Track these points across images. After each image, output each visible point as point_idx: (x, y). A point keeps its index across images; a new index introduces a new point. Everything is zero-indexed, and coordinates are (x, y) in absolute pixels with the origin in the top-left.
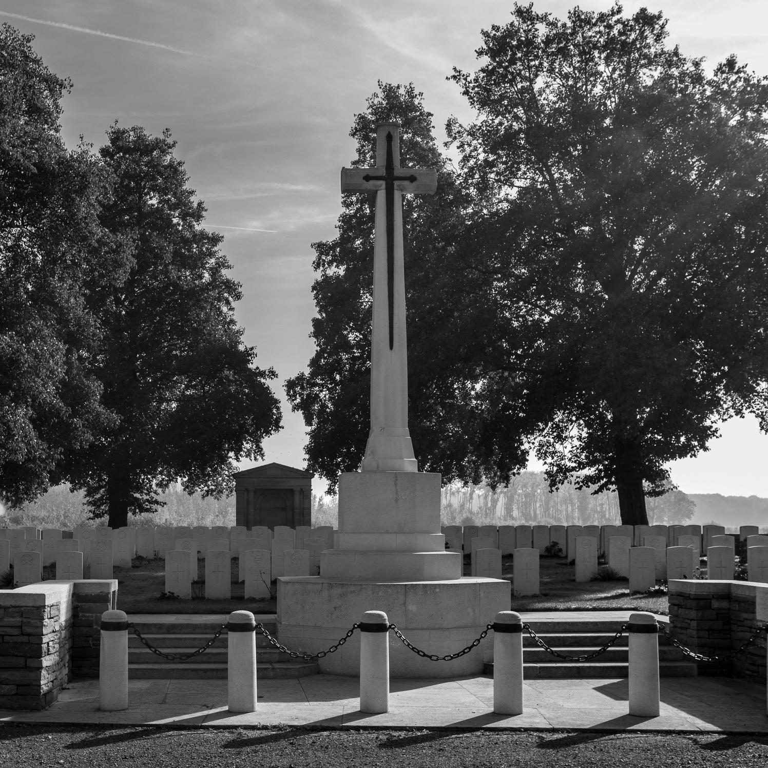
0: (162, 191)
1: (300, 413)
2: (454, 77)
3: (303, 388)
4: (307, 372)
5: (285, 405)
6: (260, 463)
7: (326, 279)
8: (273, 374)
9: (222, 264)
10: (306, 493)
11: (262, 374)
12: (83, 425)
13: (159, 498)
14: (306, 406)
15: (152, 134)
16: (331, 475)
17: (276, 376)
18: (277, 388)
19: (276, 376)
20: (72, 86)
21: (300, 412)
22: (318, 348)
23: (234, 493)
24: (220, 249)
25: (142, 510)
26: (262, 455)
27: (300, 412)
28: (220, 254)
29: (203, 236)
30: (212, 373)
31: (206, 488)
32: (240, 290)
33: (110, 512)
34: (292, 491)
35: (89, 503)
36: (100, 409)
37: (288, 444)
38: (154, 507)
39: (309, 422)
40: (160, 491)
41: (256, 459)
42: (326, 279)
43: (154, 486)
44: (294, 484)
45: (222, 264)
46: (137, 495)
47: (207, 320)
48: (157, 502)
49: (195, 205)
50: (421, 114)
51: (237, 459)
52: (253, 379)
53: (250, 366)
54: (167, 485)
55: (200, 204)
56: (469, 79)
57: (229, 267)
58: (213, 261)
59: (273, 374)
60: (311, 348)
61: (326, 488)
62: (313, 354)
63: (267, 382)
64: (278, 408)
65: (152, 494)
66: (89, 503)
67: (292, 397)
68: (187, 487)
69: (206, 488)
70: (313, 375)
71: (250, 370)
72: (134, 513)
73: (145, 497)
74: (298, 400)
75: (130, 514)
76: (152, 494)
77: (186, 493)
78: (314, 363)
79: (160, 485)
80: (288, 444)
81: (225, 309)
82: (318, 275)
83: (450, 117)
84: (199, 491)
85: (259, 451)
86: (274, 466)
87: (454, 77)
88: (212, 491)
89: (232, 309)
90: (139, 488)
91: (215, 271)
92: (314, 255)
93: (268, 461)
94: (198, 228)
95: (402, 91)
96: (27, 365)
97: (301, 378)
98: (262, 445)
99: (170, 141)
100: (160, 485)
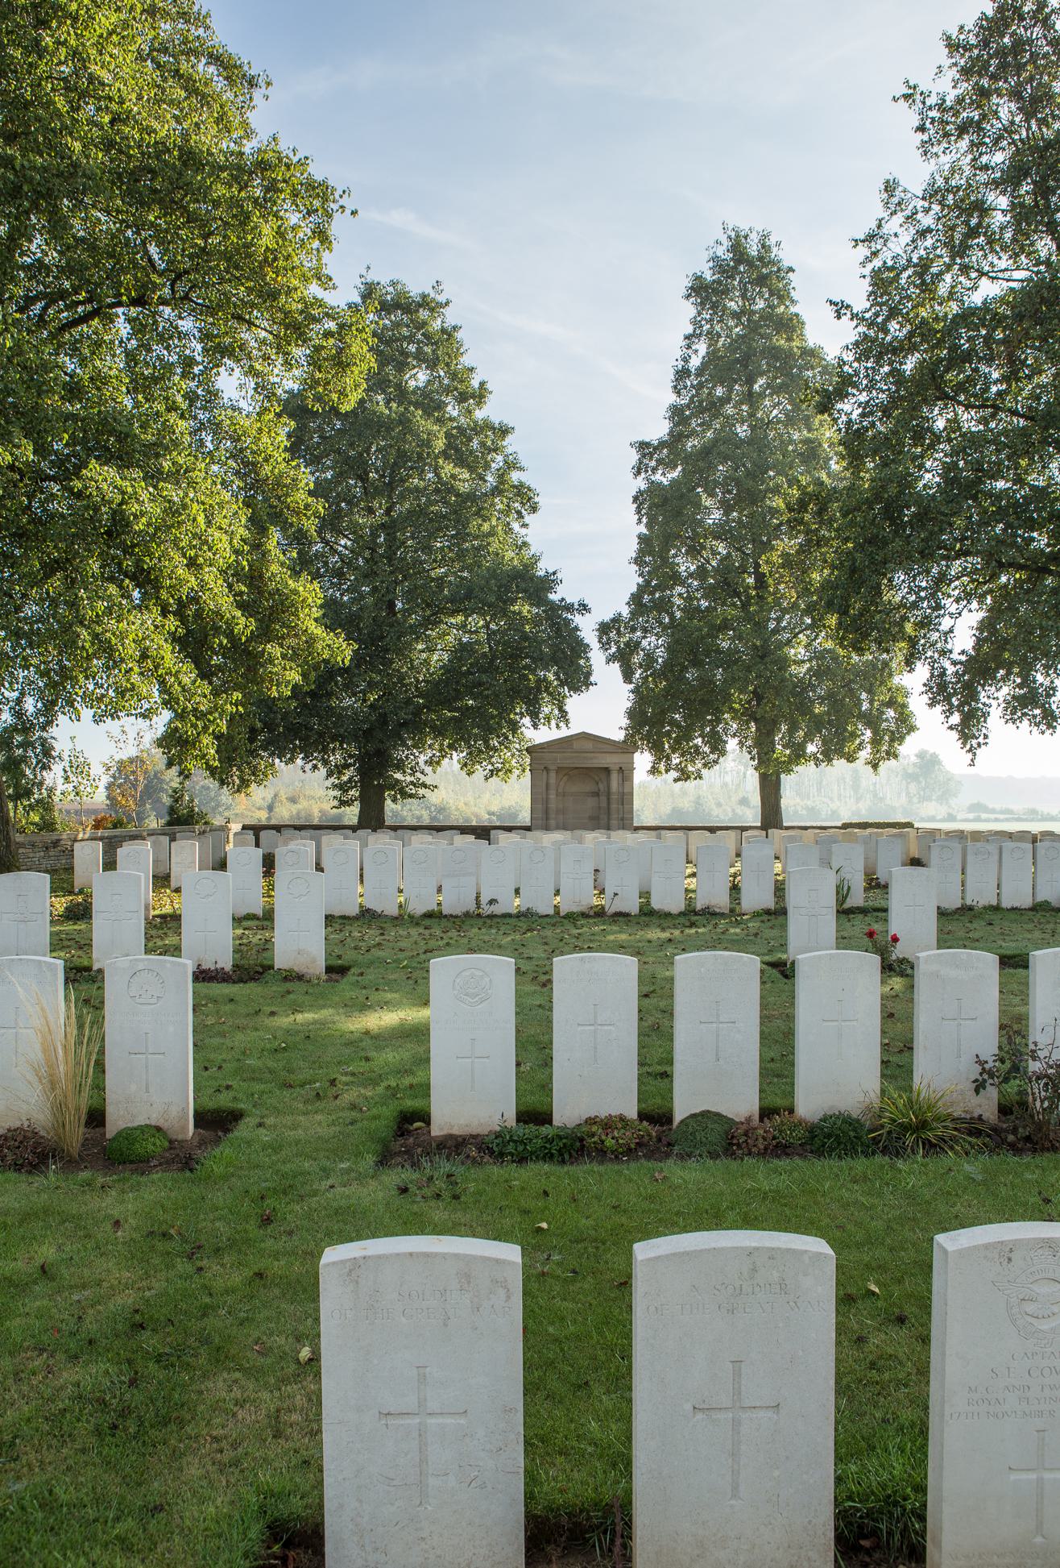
0: (432, 365)
1: (616, 667)
2: (907, 97)
3: (619, 633)
4: (625, 612)
5: (597, 657)
6: (564, 732)
7: (654, 487)
8: (584, 608)
9: (511, 465)
10: (626, 773)
11: (569, 608)
12: (284, 656)
13: (428, 780)
14: (623, 658)
15: (416, 288)
16: (657, 748)
17: (588, 611)
18: (587, 627)
19: (588, 611)
20: (269, 84)
21: (617, 665)
22: (640, 580)
23: (528, 773)
24: (511, 444)
25: (405, 795)
26: (567, 722)
27: (617, 665)
28: (510, 450)
29: (487, 425)
30: (499, 606)
31: (490, 767)
32: (536, 499)
33: (363, 798)
34: (607, 770)
35: (335, 786)
36: (319, 631)
37: (602, 707)
38: (421, 791)
39: (628, 676)
40: (428, 769)
41: (558, 727)
42: (654, 487)
43: (421, 764)
44: (611, 760)
45: (511, 465)
46: (398, 776)
47: (492, 533)
48: (425, 786)
49: (477, 386)
50: (779, 270)
51: (535, 726)
52: (558, 618)
53: (552, 596)
54: (438, 763)
55: (482, 384)
56: (929, 102)
57: (521, 469)
58: (499, 458)
59: (584, 608)
60: (631, 580)
61: (649, 766)
62: (634, 589)
63: (578, 619)
64: (588, 659)
65: (418, 774)
66: (335, 786)
67: (605, 646)
68: (465, 765)
69: (490, 767)
70: (634, 615)
71: (552, 603)
72: (394, 800)
73: (409, 779)
74: (614, 649)
75: (388, 802)
76: (418, 774)
77: (464, 773)
78: (636, 599)
79: (429, 763)
80: (602, 707)
81: (516, 526)
82: (641, 483)
83: (888, 177)
84: (480, 772)
85: (563, 715)
86: (584, 736)
87: (907, 97)
88: (499, 770)
89: (525, 526)
90: (400, 766)
91: (502, 477)
92: (634, 457)
93: (575, 729)
94: (479, 415)
95: (754, 238)
96: (144, 520)
97: (616, 620)
98: (567, 708)
99: (441, 299)
100: (429, 763)
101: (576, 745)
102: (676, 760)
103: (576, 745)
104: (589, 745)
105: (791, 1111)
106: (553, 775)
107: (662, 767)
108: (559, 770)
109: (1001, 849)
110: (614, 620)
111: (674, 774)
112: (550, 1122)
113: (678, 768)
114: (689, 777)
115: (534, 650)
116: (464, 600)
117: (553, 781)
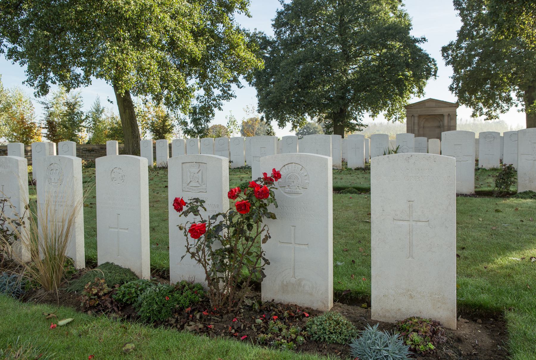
6: (422, 99)
10: (453, 117)
11: (416, 41)
34: (442, 115)
37: (440, 86)
38: (362, 128)
44: (444, 111)
48: (362, 125)
80: (440, 86)
86: (431, 100)
101: (427, 105)
102: (485, 110)
103: (427, 105)
104: (434, 104)
105: (257, 286)
106: (416, 119)
107: (478, 113)
108: (420, 116)
109: (155, 159)
110: (450, 45)
111: (484, 117)
112: (168, 278)
113: (486, 114)
114: (492, 118)
115: (408, 64)
116: (368, 42)
117: (416, 121)
